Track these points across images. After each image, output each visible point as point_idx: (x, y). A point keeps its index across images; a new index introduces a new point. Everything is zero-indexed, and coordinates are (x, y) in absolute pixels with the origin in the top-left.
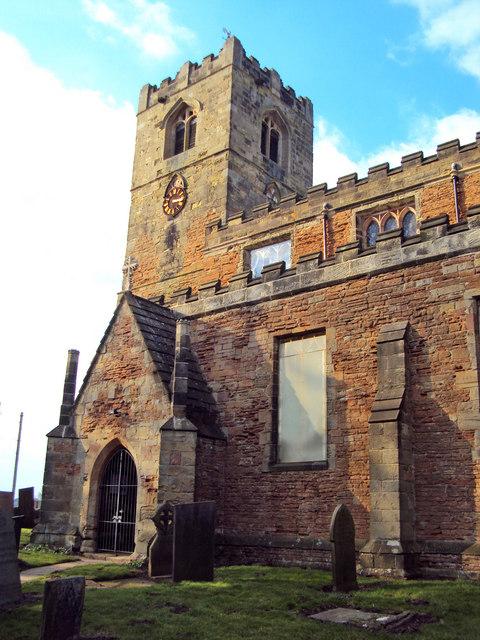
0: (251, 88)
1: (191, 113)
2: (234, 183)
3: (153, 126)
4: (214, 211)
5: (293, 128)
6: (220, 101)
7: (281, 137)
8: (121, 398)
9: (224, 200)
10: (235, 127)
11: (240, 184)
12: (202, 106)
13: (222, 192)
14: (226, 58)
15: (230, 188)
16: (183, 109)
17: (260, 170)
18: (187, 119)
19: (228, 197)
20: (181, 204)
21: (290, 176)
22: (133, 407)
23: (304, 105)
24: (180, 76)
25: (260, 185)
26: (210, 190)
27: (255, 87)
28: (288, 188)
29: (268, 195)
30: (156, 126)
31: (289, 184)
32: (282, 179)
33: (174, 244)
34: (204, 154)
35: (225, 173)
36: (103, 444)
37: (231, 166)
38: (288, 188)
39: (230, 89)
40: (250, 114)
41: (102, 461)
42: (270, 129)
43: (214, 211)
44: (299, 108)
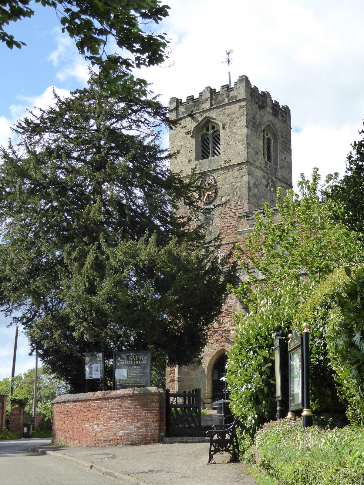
0: (256, 112)
1: (213, 128)
2: (251, 185)
3: (184, 133)
4: (239, 203)
5: (280, 134)
6: (238, 125)
7: (272, 141)
8: (224, 327)
9: (246, 197)
10: (250, 145)
11: (254, 184)
12: (224, 125)
13: (245, 191)
14: (241, 93)
15: (249, 189)
16: (207, 123)
17: (263, 170)
18: (211, 132)
19: (249, 194)
20: (213, 195)
21: (280, 170)
22: (232, 332)
23: (286, 113)
24: (203, 98)
25: (264, 182)
26: (235, 188)
27: (258, 110)
28: (279, 180)
29: (269, 188)
30: (187, 133)
31: (280, 177)
32: (275, 174)
33: (211, 222)
34: (229, 162)
35: (246, 178)
36: (214, 352)
37: (249, 173)
38: (279, 180)
39: (245, 117)
40: (256, 132)
41: (213, 362)
42: (266, 137)
43: (239, 203)
44: (282, 116)
